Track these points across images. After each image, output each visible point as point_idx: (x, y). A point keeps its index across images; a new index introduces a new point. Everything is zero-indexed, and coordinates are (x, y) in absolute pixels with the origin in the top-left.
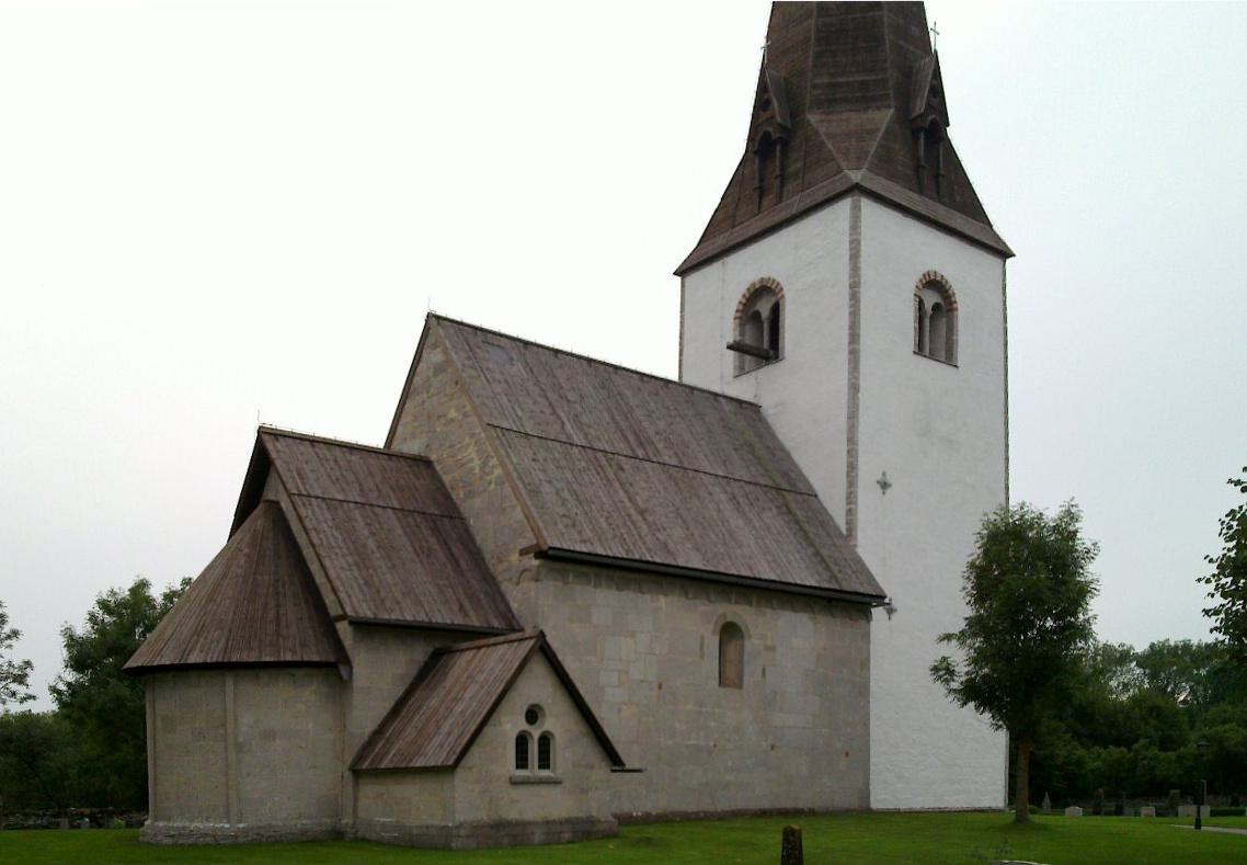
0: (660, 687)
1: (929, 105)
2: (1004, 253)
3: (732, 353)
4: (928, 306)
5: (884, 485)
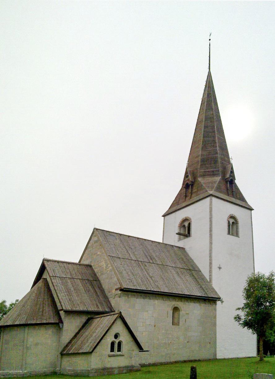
0: (155, 326)
2: (251, 209)
3: (177, 235)
5: (220, 268)
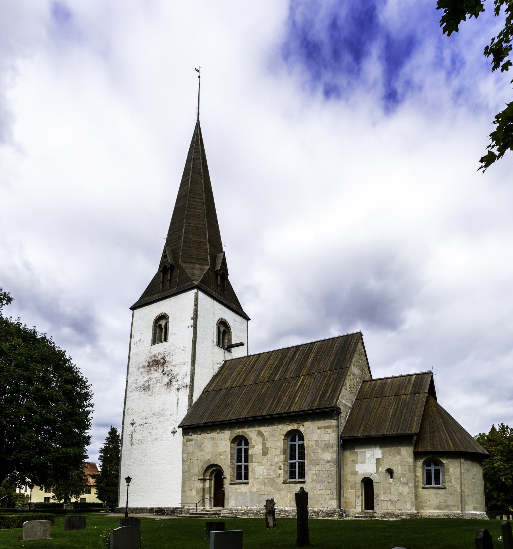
1: (221, 267)
2: (247, 319)
4: (222, 330)
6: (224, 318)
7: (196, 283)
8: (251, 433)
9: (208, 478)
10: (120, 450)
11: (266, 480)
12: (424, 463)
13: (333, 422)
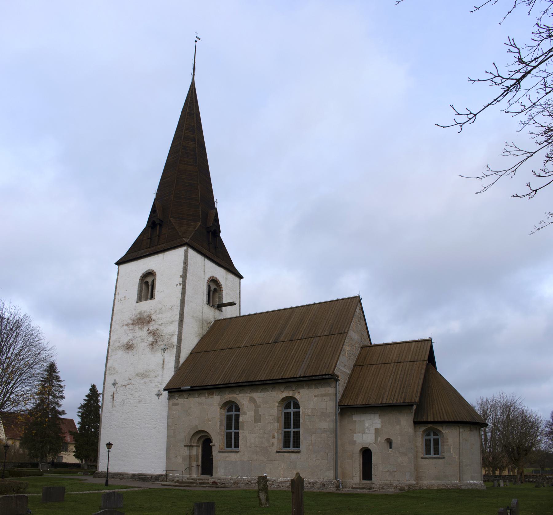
2: (240, 277)
4: (212, 288)
6: (215, 276)
7: (187, 241)
8: (243, 399)
9: (195, 444)
10: (100, 407)
11: (258, 449)
12: (424, 431)
13: (330, 390)
